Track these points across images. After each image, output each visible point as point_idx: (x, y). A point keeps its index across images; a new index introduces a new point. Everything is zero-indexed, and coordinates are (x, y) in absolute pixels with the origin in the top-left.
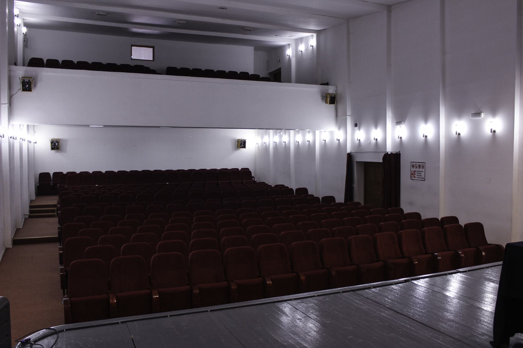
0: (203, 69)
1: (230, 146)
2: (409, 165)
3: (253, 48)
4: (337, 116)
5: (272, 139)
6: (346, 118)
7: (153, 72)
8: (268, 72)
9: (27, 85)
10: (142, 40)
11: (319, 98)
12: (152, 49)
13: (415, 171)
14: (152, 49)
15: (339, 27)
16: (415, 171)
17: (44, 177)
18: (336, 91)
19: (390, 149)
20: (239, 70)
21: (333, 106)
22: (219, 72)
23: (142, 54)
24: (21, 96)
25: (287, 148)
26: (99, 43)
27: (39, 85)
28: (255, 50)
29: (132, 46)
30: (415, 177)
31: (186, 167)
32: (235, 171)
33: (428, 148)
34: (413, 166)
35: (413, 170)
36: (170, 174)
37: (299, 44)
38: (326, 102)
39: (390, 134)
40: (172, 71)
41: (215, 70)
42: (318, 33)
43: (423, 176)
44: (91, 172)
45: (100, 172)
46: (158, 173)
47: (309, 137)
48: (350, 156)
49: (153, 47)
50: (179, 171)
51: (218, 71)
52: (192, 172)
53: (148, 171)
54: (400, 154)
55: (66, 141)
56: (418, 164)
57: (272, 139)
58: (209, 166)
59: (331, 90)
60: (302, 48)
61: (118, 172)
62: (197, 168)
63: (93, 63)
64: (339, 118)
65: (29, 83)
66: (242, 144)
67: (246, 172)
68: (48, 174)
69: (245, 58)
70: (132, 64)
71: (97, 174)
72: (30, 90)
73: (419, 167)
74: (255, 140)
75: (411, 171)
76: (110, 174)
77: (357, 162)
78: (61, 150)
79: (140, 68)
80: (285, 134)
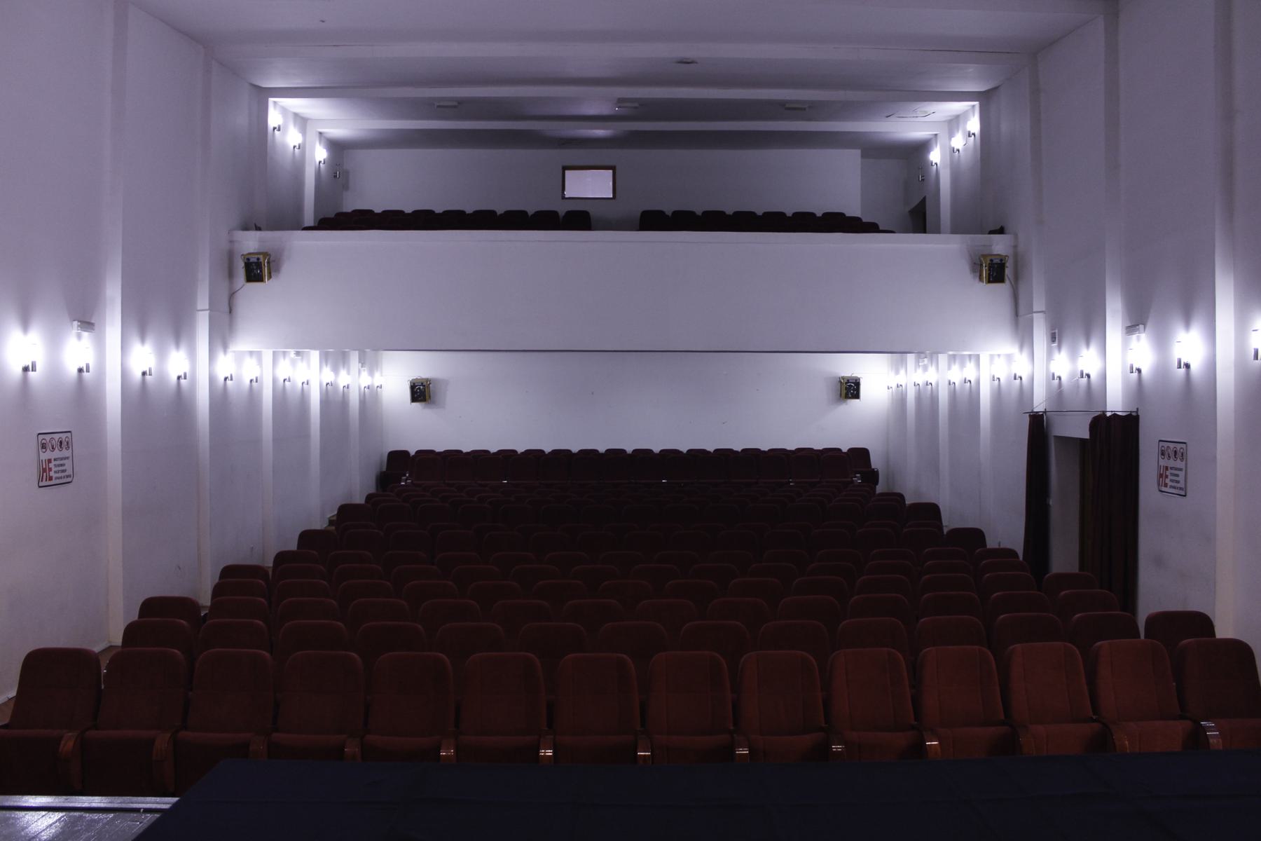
0: (729, 210)
1: (823, 392)
2: (1155, 451)
3: (858, 152)
4: (1016, 314)
5: (916, 376)
6: (1032, 321)
7: (872, 228)
8: (908, 209)
9: (256, 271)
10: (584, 152)
11: (964, 266)
12: (567, 172)
13: (50, 461)
14: (567, 172)
15: (1019, 73)
16: (50, 461)
17: (398, 458)
18: (1015, 247)
19: (1116, 402)
20: (819, 207)
21: (1002, 290)
22: (767, 215)
23: (591, 185)
24: (251, 293)
25: (180, 400)
26: (498, 164)
27: (286, 268)
28: (863, 156)
29: (565, 168)
30: (1166, 485)
31: (791, 444)
32: (831, 455)
33: (1192, 396)
34: (44, 446)
35: (1163, 463)
36: (670, 457)
37: (949, 131)
38: (981, 279)
39: (1115, 362)
40: (652, 221)
41: (760, 212)
42: (985, 99)
43: (1182, 485)
44: (845, 449)
45: (650, 451)
46: (643, 455)
47: (970, 372)
48: (1038, 423)
49: (613, 168)
50: (474, 452)
51: (767, 214)
52: (724, 455)
53: (783, 452)
54: (1137, 418)
55: (436, 380)
56: (1172, 445)
57: (916, 376)
58: (765, 444)
59: (999, 246)
60: (958, 142)
61: (690, 451)
62: (738, 447)
63: (477, 213)
64: (1021, 319)
65: (259, 265)
66: (851, 389)
67: (860, 455)
68: (406, 453)
69: (839, 181)
70: (562, 209)
71: (507, 457)
72: (259, 279)
73: (1174, 452)
74: (881, 379)
75: (40, 462)
76: (534, 457)
77: (1056, 437)
78: (434, 403)
79: (578, 219)
80: (143, 340)
